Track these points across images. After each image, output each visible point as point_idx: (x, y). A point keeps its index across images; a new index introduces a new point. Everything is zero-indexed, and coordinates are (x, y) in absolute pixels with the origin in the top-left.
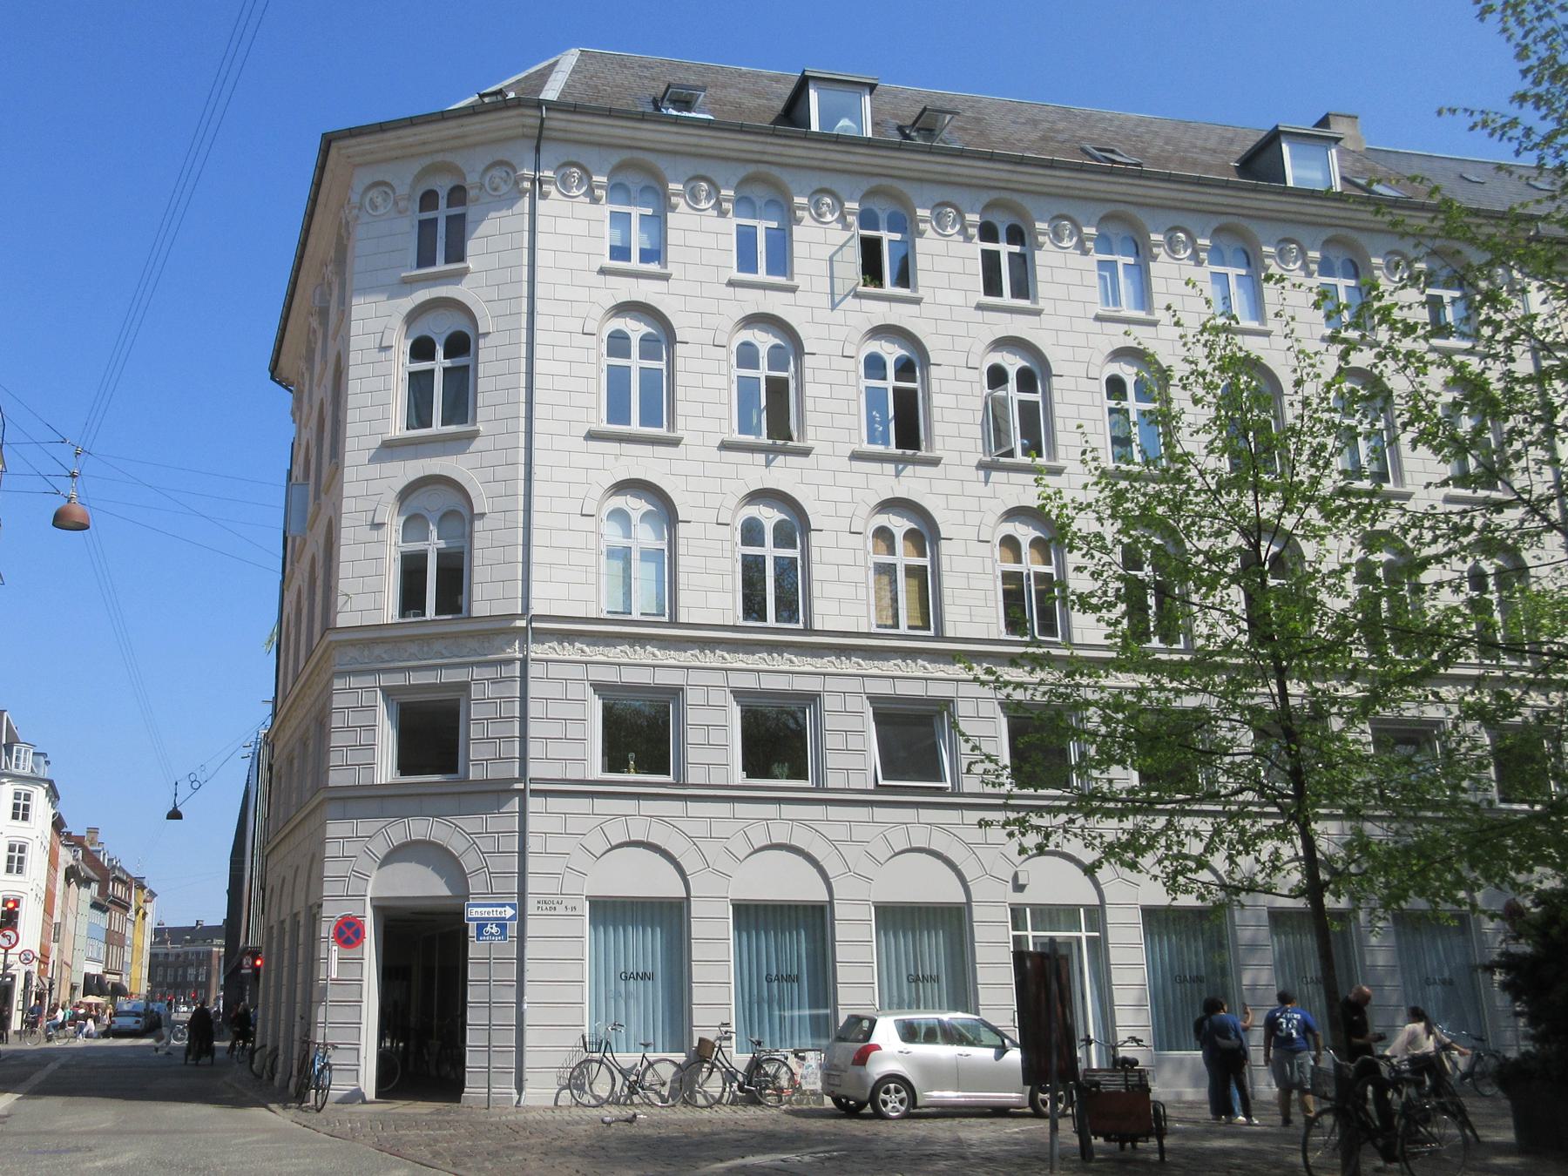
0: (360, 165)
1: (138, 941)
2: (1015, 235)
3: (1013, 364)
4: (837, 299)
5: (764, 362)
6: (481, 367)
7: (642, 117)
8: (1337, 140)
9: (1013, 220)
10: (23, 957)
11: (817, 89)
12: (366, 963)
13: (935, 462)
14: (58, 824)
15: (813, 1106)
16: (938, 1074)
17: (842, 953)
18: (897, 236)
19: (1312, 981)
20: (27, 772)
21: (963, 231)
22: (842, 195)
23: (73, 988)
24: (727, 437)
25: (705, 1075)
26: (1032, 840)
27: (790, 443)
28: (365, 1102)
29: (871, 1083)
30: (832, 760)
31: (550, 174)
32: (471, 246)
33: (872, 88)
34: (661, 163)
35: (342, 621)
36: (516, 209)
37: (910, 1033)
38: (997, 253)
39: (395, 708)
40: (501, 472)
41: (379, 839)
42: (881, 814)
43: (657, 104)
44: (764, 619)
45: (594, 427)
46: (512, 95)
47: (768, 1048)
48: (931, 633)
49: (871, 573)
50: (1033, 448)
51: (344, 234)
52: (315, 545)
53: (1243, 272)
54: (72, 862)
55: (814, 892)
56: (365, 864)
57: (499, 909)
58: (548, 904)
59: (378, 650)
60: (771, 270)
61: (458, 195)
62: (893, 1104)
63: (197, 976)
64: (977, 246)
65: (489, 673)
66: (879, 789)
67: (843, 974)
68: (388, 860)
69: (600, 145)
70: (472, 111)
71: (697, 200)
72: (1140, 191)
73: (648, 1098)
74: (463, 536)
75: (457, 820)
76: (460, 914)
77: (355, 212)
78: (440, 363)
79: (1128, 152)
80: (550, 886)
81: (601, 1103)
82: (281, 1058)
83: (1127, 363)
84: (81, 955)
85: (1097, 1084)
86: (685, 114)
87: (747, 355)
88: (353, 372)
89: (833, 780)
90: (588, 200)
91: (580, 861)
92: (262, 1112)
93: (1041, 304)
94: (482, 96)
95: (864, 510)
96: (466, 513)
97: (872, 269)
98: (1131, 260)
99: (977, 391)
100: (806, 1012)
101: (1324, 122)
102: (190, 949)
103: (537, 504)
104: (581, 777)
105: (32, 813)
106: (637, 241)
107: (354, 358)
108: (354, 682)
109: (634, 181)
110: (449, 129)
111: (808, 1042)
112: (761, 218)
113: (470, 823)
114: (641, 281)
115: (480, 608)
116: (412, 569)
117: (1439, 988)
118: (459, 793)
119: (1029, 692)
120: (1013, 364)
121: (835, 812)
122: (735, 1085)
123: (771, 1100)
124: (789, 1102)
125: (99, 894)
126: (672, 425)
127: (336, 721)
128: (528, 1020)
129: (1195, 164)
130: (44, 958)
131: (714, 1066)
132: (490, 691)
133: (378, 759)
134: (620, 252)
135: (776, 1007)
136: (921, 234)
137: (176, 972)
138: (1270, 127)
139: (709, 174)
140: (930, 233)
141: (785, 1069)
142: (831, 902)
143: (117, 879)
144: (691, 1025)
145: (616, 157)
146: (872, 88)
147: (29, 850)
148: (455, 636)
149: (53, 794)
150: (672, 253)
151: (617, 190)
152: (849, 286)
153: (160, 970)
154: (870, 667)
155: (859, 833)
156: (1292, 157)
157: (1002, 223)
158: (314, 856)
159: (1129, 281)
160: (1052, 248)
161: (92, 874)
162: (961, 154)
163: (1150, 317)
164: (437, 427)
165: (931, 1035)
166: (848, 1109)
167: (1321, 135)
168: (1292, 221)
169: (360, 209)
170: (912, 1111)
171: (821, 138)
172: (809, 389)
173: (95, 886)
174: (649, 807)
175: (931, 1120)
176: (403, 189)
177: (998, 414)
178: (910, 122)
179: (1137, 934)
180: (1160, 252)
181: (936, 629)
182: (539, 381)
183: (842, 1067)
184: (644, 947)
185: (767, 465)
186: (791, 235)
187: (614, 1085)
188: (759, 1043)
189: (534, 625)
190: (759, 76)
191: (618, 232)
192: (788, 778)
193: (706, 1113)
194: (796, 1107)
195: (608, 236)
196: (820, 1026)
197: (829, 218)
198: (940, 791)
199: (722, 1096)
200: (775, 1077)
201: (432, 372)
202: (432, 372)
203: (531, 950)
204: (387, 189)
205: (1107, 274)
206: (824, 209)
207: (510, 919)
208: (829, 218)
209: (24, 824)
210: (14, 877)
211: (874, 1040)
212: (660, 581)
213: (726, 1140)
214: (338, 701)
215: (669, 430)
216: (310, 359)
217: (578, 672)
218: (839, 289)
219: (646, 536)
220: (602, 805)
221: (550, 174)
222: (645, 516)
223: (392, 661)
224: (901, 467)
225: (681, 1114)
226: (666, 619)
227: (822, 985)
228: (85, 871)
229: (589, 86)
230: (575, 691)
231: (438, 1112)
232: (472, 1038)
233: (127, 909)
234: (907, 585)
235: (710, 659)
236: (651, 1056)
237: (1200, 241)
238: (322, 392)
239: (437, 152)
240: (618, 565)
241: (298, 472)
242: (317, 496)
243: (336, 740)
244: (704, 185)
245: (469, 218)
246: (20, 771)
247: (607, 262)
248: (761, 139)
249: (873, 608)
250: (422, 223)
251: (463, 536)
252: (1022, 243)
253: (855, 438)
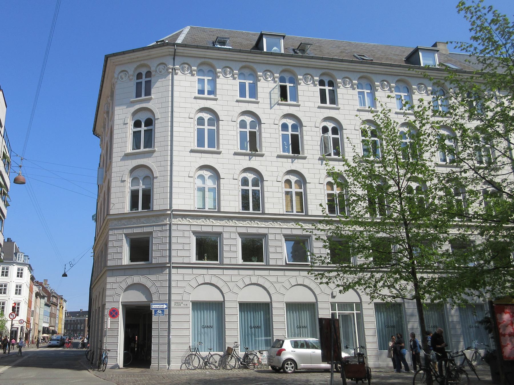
1: (61, 316)
2: (331, 84)
3: (330, 125)
4: (272, 105)
5: (248, 126)
7: (208, 48)
8: (438, 51)
10: (20, 322)
12: (120, 323)
13: (305, 158)
14: (32, 278)
15: (265, 369)
16: (304, 358)
17: (275, 319)
19: (431, 327)
20: (22, 262)
21: (313, 83)
22: (273, 72)
23: (39, 332)
24: (236, 151)
25: (230, 359)
26: (325, 280)
27: (257, 153)
28: (119, 368)
30: (271, 256)
31: (178, 67)
32: (153, 91)
35: (112, 212)
40: (163, 163)
41: (124, 283)
42: (288, 273)
43: (214, 44)
44: (249, 210)
45: (193, 148)
47: (250, 350)
48: (304, 214)
49: (326, 196)
50: (337, 153)
51: (113, 88)
52: (105, 189)
53: (406, 94)
54: (38, 290)
55: (266, 299)
56: (119, 291)
57: (162, 305)
58: (178, 303)
59: (123, 222)
60: (250, 97)
61: (149, 74)
62: (290, 368)
63: (80, 327)
65: (159, 228)
66: (287, 265)
67: (275, 326)
68: (126, 289)
70: (153, 47)
75: (149, 276)
76: (149, 307)
77: (116, 80)
78: (143, 128)
79: (369, 56)
80: (179, 298)
81: (196, 368)
82: (95, 354)
83: (443, 130)
84: (41, 321)
85: (348, 361)
86: (223, 47)
87: (243, 124)
88: (115, 132)
89: (272, 262)
91: (188, 289)
94: (157, 42)
95: (281, 174)
96: (151, 177)
97: (283, 95)
98: (369, 91)
99: (318, 135)
100: (263, 338)
101: (435, 45)
103: (174, 173)
104: (189, 262)
105: (24, 275)
106: (207, 88)
107: (116, 127)
108: (116, 232)
109: (205, 68)
110: (145, 53)
111: (264, 348)
112: (247, 80)
113: (153, 277)
116: (134, 195)
117: (474, 329)
118: (137, 268)
120: (330, 125)
121: (272, 273)
122: (240, 362)
123: (252, 367)
124: (257, 368)
125: (47, 301)
126: (218, 147)
129: (391, 59)
130: (28, 322)
131: (232, 356)
133: (123, 257)
134: (201, 92)
135: (253, 336)
136: (300, 84)
137: (74, 326)
139: (387, 80)
140: (302, 84)
141: (256, 357)
142: (271, 302)
144: (225, 343)
145: (200, 61)
147: (22, 287)
148: (148, 216)
149: (30, 269)
150: (218, 92)
151: (200, 72)
152: (276, 101)
156: (422, 57)
157: (326, 80)
159: (369, 98)
162: (312, 58)
164: (142, 149)
166: (276, 370)
167: (434, 49)
170: (296, 370)
171: (267, 54)
172: (263, 135)
173: (46, 299)
174: (211, 272)
176: (131, 72)
178: (297, 47)
179: (372, 312)
181: (305, 212)
183: (274, 356)
184: (210, 317)
185: (292, 163)
187: (199, 363)
188: (247, 349)
189: (173, 213)
190: (249, 34)
191: (200, 85)
193: (229, 371)
195: (197, 86)
196: (268, 343)
197: (269, 79)
198: (307, 265)
199: (235, 366)
200: (253, 359)
201: (141, 131)
203: (172, 319)
204: (126, 73)
205: (361, 96)
206: (268, 76)
207: (165, 309)
208: (269, 79)
209: (21, 278)
210: (18, 296)
211: (283, 347)
213: (231, 380)
214: (111, 238)
216: (104, 128)
217: (188, 228)
218: (273, 102)
219: (210, 184)
220: (196, 271)
221: (178, 67)
222: (210, 177)
225: (221, 372)
226: (217, 210)
228: (42, 293)
229: (192, 38)
230: (233, 236)
231: (142, 371)
232: (153, 347)
233: (57, 306)
236: (212, 353)
237: (392, 85)
238: (107, 139)
239: (142, 60)
240: (201, 193)
241: (101, 164)
242: (106, 172)
243: (110, 251)
244: (228, 69)
245: (152, 82)
246: (19, 261)
247: (197, 95)
249: (285, 206)
252: (333, 87)
253: (278, 150)
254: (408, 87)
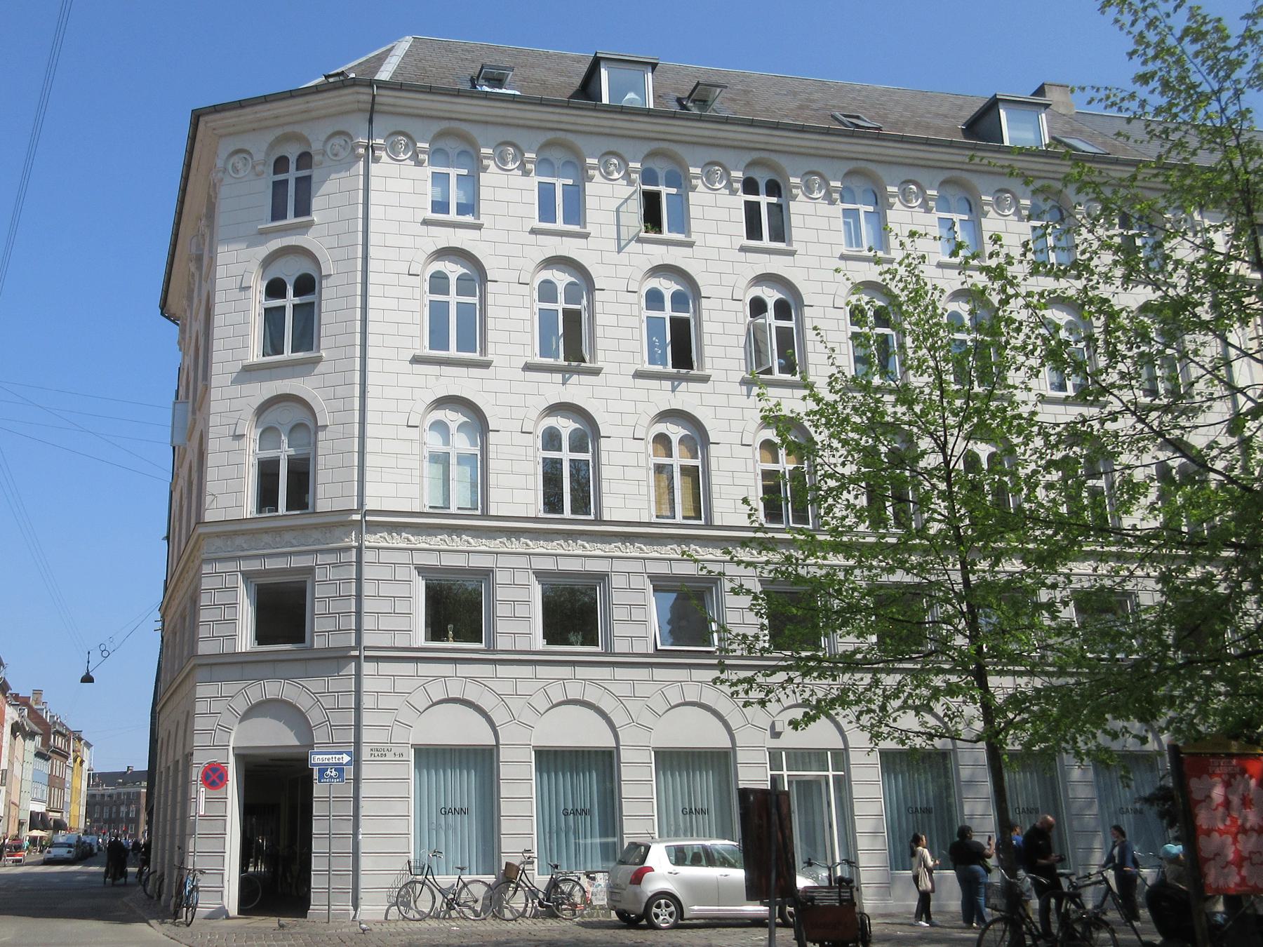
0: (226, 136)
1: (76, 783)
2: (774, 188)
3: (771, 296)
4: (623, 243)
6: (323, 303)
7: (458, 93)
8: (1047, 106)
11: (607, 68)
12: (229, 802)
15: (602, 919)
17: (626, 791)
18: (674, 191)
21: (729, 185)
23: (21, 824)
25: (511, 892)
27: (583, 364)
28: (228, 918)
29: (645, 900)
30: (618, 630)
31: (381, 141)
32: (316, 203)
33: (654, 66)
34: (474, 131)
35: (209, 516)
36: (353, 171)
37: (680, 857)
38: (758, 204)
39: (253, 589)
40: (340, 391)
42: (660, 674)
43: (473, 82)
45: (418, 352)
46: (353, 75)
48: (702, 522)
49: (760, 477)
50: (789, 367)
51: (212, 193)
52: (192, 456)
53: (966, 217)
54: (17, 718)
56: (227, 719)
57: (337, 756)
58: (380, 752)
59: (239, 541)
61: (305, 159)
62: (664, 917)
63: (128, 813)
64: (742, 198)
65: (330, 558)
67: (627, 808)
68: (246, 716)
69: (734, 147)
70: (316, 90)
71: (505, 162)
72: (878, 150)
73: (463, 912)
74: (309, 444)
75: (304, 682)
77: (220, 175)
78: (290, 300)
79: (872, 118)
80: (381, 736)
81: (424, 917)
82: (166, 881)
84: (26, 796)
86: (497, 90)
87: (547, 290)
88: (218, 309)
89: (620, 646)
90: (413, 163)
91: (406, 715)
92: (143, 926)
93: (795, 246)
94: (327, 77)
96: (311, 426)
97: (652, 217)
98: (871, 209)
100: (598, 840)
101: (1040, 91)
102: (122, 790)
103: (370, 417)
104: (407, 645)
107: (219, 297)
108: (219, 567)
109: (452, 146)
110: (298, 104)
111: (598, 865)
112: (559, 176)
113: (315, 685)
114: (773, 257)
115: (323, 505)
116: (267, 472)
119: (759, 570)
120: (771, 296)
121: (620, 673)
122: (536, 901)
123: (568, 914)
124: (582, 916)
125: (42, 745)
126: (484, 351)
127: (204, 600)
128: (362, 849)
129: (927, 127)
131: (518, 885)
132: (332, 574)
133: (239, 632)
134: (440, 206)
136: (891, 206)
137: (111, 809)
138: (993, 94)
142: (618, 748)
143: (58, 733)
144: (500, 852)
145: (437, 127)
146: (654, 66)
148: (303, 528)
151: (438, 155)
152: (633, 232)
153: (97, 808)
154: (651, 551)
155: (641, 690)
157: (762, 178)
158: (188, 712)
160: (389, 161)
161: (36, 728)
162: (727, 121)
163: (887, 256)
164: (288, 354)
165: (696, 860)
166: (630, 920)
167: (1037, 100)
168: (591, 133)
169: (224, 172)
170: (680, 922)
171: (609, 109)
172: (600, 319)
173: (38, 739)
174: (464, 670)
175: (695, 930)
176: (259, 156)
177: (759, 337)
178: (687, 94)
179: (875, 773)
180: (895, 201)
181: (706, 518)
182: (371, 315)
183: (623, 886)
185: (673, 391)
186: (688, 199)
187: (434, 902)
188: (556, 867)
189: (367, 518)
190: (563, 57)
192: (582, 644)
193: (510, 925)
194: (587, 919)
195: (429, 192)
196: (608, 852)
197: (616, 175)
199: (525, 910)
200: (570, 894)
201: (284, 308)
202: (284, 308)
205: (851, 221)
206: (612, 168)
208: (616, 175)
211: (648, 863)
212: (474, 485)
214: (206, 584)
215: (481, 355)
216: (190, 298)
218: (624, 235)
219: (462, 444)
220: (424, 668)
221: (381, 141)
222: (461, 427)
223: (252, 549)
224: (676, 383)
225: (490, 926)
226: (479, 512)
227: (610, 818)
228: (29, 725)
233: (67, 758)
234: (683, 482)
235: (516, 545)
236: (466, 878)
238: (197, 326)
240: (438, 469)
241: (182, 392)
242: (194, 413)
243: (204, 616)
244: (511, 150)
245: (314, 180)
247: (430, 215)
248: (558, 110)
250: (275, 184)
251: (309, 444)
252: (780, 196)
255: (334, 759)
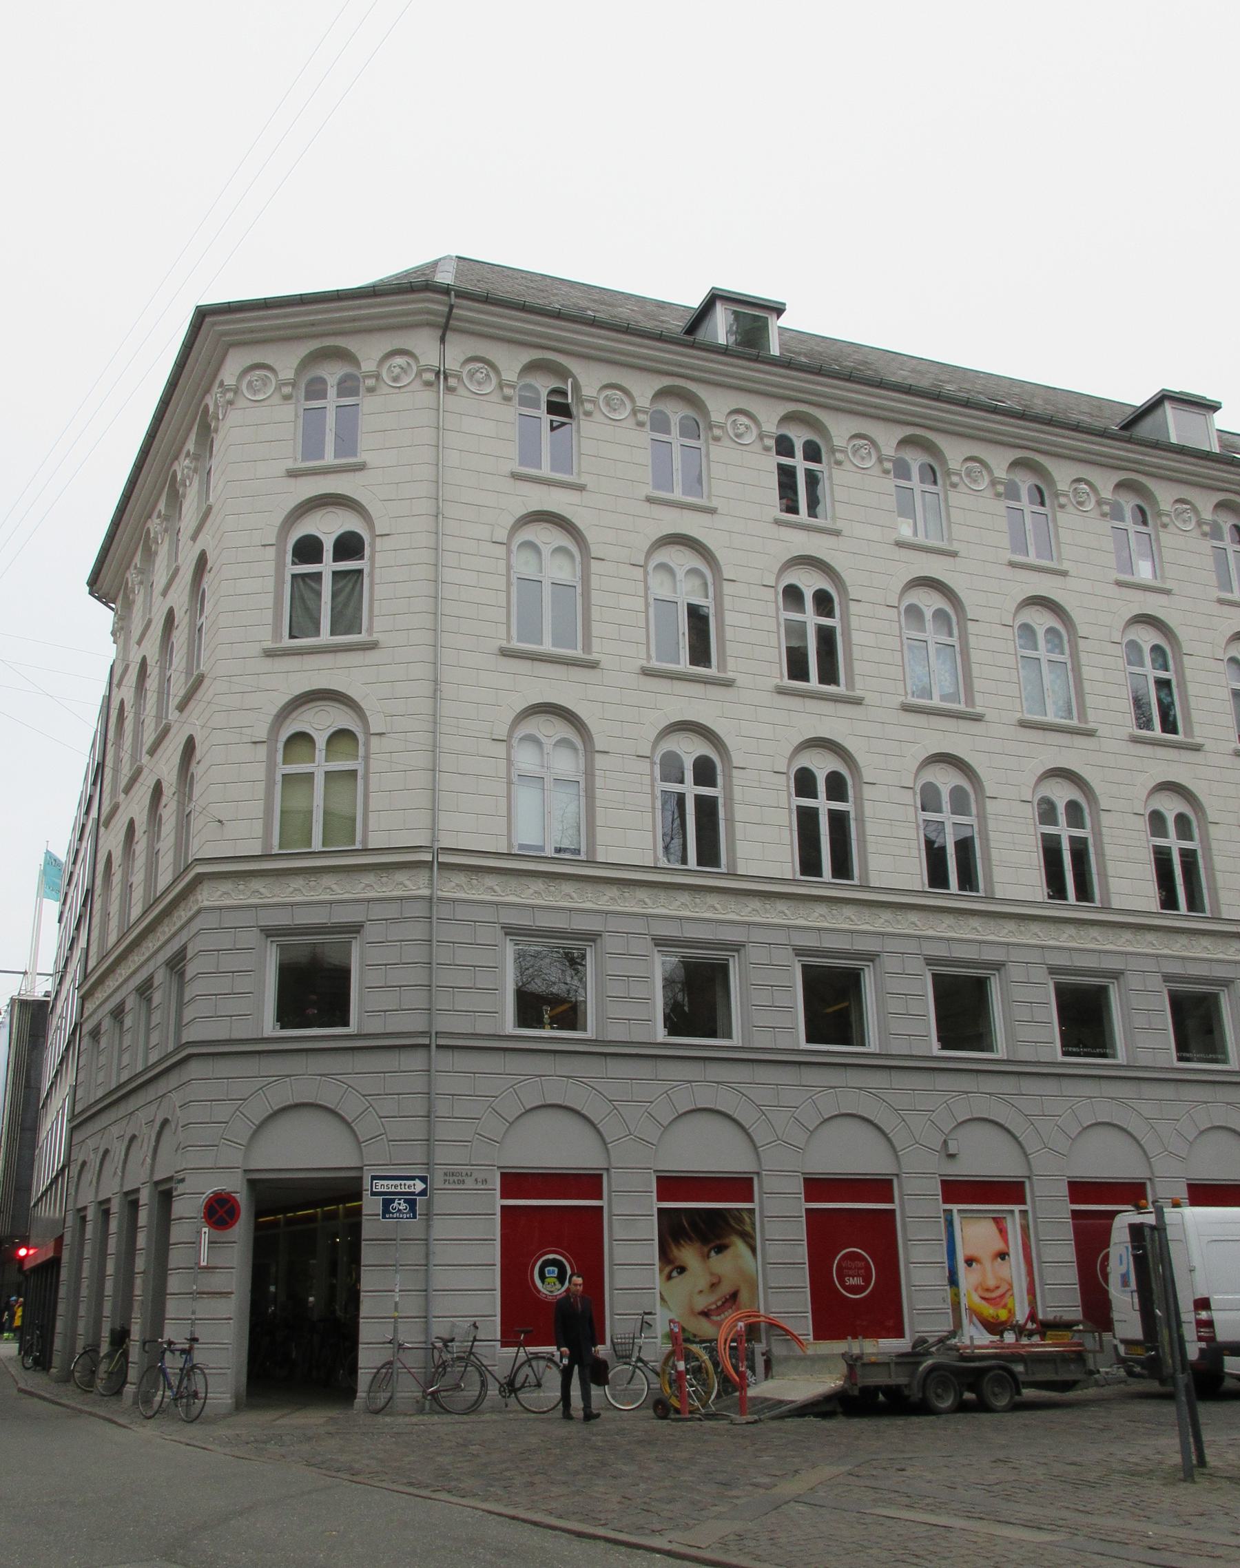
9: (810, 436)
57: (408, 1183)
77: (230, 396)
120: (810, 583)
157: (799, 437)
164: (325, 636)
254: (1042, 486)
255: (403, 1186)
